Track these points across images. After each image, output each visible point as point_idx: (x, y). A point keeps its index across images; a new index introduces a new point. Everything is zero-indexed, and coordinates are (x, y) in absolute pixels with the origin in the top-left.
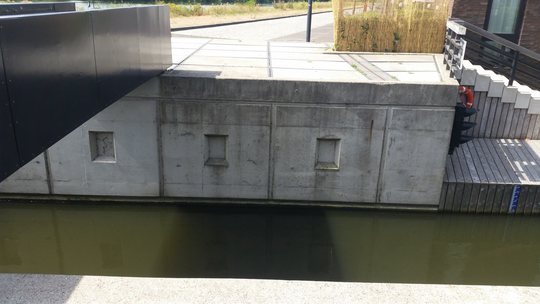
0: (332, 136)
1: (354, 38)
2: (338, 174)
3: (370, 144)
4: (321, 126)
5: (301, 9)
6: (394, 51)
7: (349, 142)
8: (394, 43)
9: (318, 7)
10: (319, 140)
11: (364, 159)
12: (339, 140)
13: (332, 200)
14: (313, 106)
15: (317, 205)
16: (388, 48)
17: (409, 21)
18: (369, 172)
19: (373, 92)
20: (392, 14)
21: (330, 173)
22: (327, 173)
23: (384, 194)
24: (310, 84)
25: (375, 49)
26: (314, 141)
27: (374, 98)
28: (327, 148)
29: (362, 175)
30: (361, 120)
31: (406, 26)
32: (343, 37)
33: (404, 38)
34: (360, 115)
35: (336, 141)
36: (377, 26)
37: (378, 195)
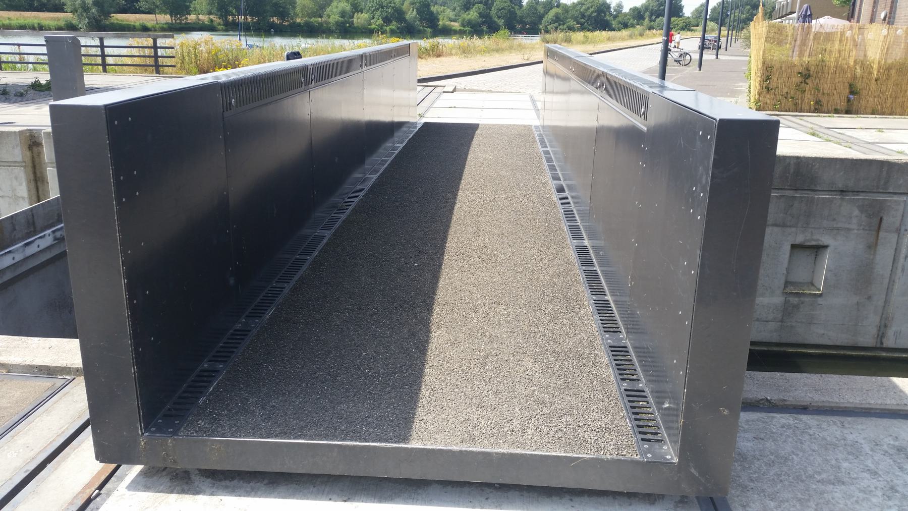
0: (814, 240)
1: (785, 90)
2: (820, 300)
3: (875, 254)
4: (800, 225)
5: (584, 43)
6: (848, 112)
7: (840, 250)
8: (849, 100)
9: (609, 39)
10: (794, 247)
11: (862, 277)
12: (826, 247)
13: (806, 342)
14: (789, 193)
15: (782, 349)
16: (839, 107)
17: (875, 66)
18: (869, 298)
19: (885, 173)
20: (847, 55)
21: (807, 299)
22: (802, 299)
23: (890, 333)
24: (788, 160)
25: (818, 108)
26: (787, 248)
27: (886, 183)
28: (804, 259)
29: (858, 303)
30: (863, 216)
31: (870, 73)
32: (768, 89)
33: (864, 92)
34: (862, 209)
35: (818, 249)
36: (823, 73)
37: (881, 336)
